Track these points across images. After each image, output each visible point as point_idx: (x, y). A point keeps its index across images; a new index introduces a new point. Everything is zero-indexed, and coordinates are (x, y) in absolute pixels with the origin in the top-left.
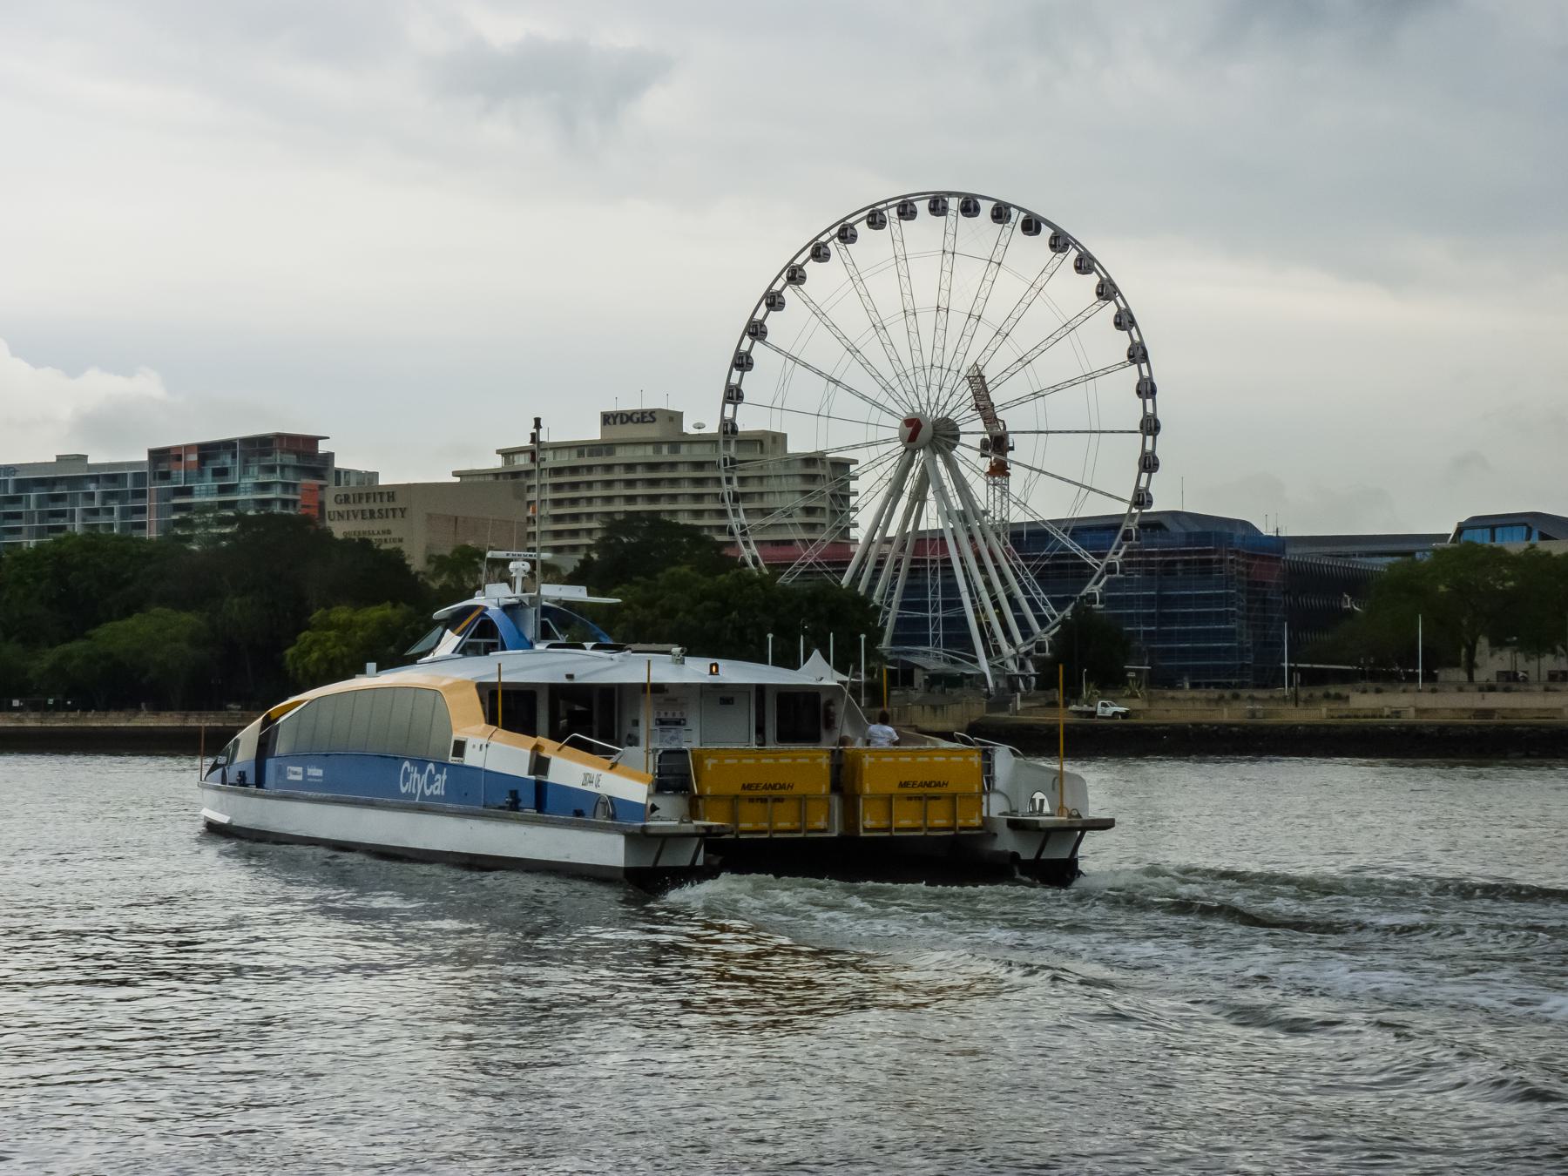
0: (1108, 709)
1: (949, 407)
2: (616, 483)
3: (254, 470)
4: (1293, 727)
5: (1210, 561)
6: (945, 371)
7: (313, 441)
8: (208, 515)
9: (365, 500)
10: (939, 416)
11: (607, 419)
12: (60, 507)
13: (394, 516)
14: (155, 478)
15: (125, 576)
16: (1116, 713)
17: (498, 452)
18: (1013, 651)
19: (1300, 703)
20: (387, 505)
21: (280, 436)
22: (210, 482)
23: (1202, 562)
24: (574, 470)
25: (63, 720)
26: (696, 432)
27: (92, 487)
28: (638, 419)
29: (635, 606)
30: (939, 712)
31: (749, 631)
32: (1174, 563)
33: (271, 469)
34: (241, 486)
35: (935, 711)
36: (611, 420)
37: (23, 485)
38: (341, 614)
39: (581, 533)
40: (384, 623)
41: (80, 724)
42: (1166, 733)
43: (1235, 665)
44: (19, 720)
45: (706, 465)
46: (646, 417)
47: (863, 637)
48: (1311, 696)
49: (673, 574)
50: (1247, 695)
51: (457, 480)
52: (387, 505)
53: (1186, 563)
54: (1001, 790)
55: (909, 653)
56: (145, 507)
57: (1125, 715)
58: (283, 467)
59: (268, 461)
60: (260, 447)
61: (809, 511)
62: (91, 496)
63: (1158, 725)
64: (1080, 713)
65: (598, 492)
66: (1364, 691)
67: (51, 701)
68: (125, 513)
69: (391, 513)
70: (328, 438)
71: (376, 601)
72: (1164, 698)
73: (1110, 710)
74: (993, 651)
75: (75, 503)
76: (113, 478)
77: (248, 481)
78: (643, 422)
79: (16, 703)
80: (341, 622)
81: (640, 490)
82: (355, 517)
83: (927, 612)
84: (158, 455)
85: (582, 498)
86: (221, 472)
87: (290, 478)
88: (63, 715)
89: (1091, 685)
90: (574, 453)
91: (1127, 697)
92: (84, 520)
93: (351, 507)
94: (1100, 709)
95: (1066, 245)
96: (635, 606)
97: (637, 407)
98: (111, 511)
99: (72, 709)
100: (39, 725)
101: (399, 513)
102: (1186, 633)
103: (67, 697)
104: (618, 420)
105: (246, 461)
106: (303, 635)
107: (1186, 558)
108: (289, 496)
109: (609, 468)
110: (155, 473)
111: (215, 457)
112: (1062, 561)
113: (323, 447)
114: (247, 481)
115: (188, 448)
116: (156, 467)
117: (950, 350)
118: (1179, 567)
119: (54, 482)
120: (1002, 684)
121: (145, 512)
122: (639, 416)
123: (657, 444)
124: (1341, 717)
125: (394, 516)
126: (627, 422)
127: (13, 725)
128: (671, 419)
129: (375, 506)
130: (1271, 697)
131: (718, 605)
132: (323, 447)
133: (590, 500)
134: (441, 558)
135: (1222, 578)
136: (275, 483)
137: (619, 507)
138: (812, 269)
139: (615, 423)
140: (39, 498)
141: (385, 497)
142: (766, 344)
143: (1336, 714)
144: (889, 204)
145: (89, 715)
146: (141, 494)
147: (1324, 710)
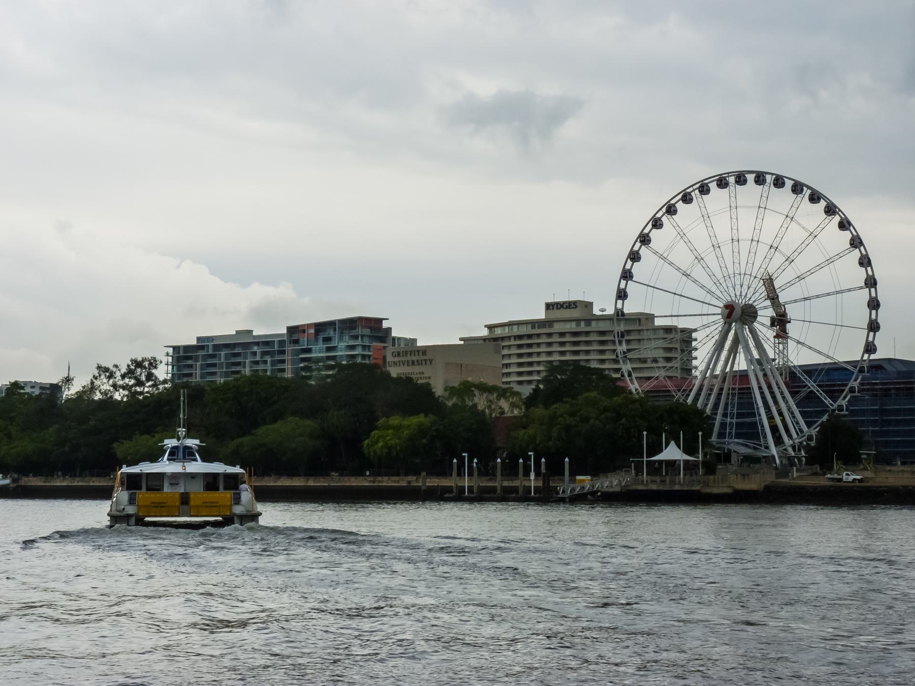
0: (850, 477)
3: (346, 338)
6: (742, 276)
7: (380, 321)
8: (320, 364)
11: (549, 306)
12: (238, 360)
13: (426, 364)
14: (290, 343)
16: (854, 479)
17: (486, 326)
18: (791, 442)
20: (422, 358)
21: (361, 319)
22: (321, 345)
23: (907, 389)
24: (530, 336)
26: (601, 313)
27: (255, 348)
28: (567, 306)
31: (632, 430)
32: (890, 389)
33: (355, 337)
34: (339, 347)
35: (744, 478)
36: (551, 307)
37: (217, 347)
38: (395, 420)
47: (700, 433)
51: (462, 342)
52: (422, 358)
53: (897, 389)
57: (860, 481)
58: (362, 336)
59: (354, 333)
60: (350, 324)
62: (255, 354)
63: (881, 487)
64: (833, 479)
65: (543, 349)
68: (274, 363)
72: (884, 470)
73: (851, 478)
76: (267, 343)
77: (342, 345)
78: (570, 308)
81: (568, 348)
82: (404, 364)
84: (292, 330)
85: (534, 353)
86: (328, 339)
89: (839, 463)
90: (530, 326)
91: (862, 470)
92: (251, 367)
94: (845, 477)
96: (565, 415)
98: (266, 362)
101: (428, 362)
104: (555, 307)
107: (898, 386)
108: (367, 353)
109: (550, 335)
110: (290, 340)
111: (324, 331)
113: (385, 325)
115: (309, 326)
116: (291, 337)
118: (893, 392)
119: (234, 346)
122: (568, 304)
123: (578, 321)
125: (426, 364)
126: (560, 308)
129: (415, 358)
132: (385, 325)
133: (539, 354)
139: (553, 309)
140: (226, 355)
141: (421, 352)
146: (283, 352)
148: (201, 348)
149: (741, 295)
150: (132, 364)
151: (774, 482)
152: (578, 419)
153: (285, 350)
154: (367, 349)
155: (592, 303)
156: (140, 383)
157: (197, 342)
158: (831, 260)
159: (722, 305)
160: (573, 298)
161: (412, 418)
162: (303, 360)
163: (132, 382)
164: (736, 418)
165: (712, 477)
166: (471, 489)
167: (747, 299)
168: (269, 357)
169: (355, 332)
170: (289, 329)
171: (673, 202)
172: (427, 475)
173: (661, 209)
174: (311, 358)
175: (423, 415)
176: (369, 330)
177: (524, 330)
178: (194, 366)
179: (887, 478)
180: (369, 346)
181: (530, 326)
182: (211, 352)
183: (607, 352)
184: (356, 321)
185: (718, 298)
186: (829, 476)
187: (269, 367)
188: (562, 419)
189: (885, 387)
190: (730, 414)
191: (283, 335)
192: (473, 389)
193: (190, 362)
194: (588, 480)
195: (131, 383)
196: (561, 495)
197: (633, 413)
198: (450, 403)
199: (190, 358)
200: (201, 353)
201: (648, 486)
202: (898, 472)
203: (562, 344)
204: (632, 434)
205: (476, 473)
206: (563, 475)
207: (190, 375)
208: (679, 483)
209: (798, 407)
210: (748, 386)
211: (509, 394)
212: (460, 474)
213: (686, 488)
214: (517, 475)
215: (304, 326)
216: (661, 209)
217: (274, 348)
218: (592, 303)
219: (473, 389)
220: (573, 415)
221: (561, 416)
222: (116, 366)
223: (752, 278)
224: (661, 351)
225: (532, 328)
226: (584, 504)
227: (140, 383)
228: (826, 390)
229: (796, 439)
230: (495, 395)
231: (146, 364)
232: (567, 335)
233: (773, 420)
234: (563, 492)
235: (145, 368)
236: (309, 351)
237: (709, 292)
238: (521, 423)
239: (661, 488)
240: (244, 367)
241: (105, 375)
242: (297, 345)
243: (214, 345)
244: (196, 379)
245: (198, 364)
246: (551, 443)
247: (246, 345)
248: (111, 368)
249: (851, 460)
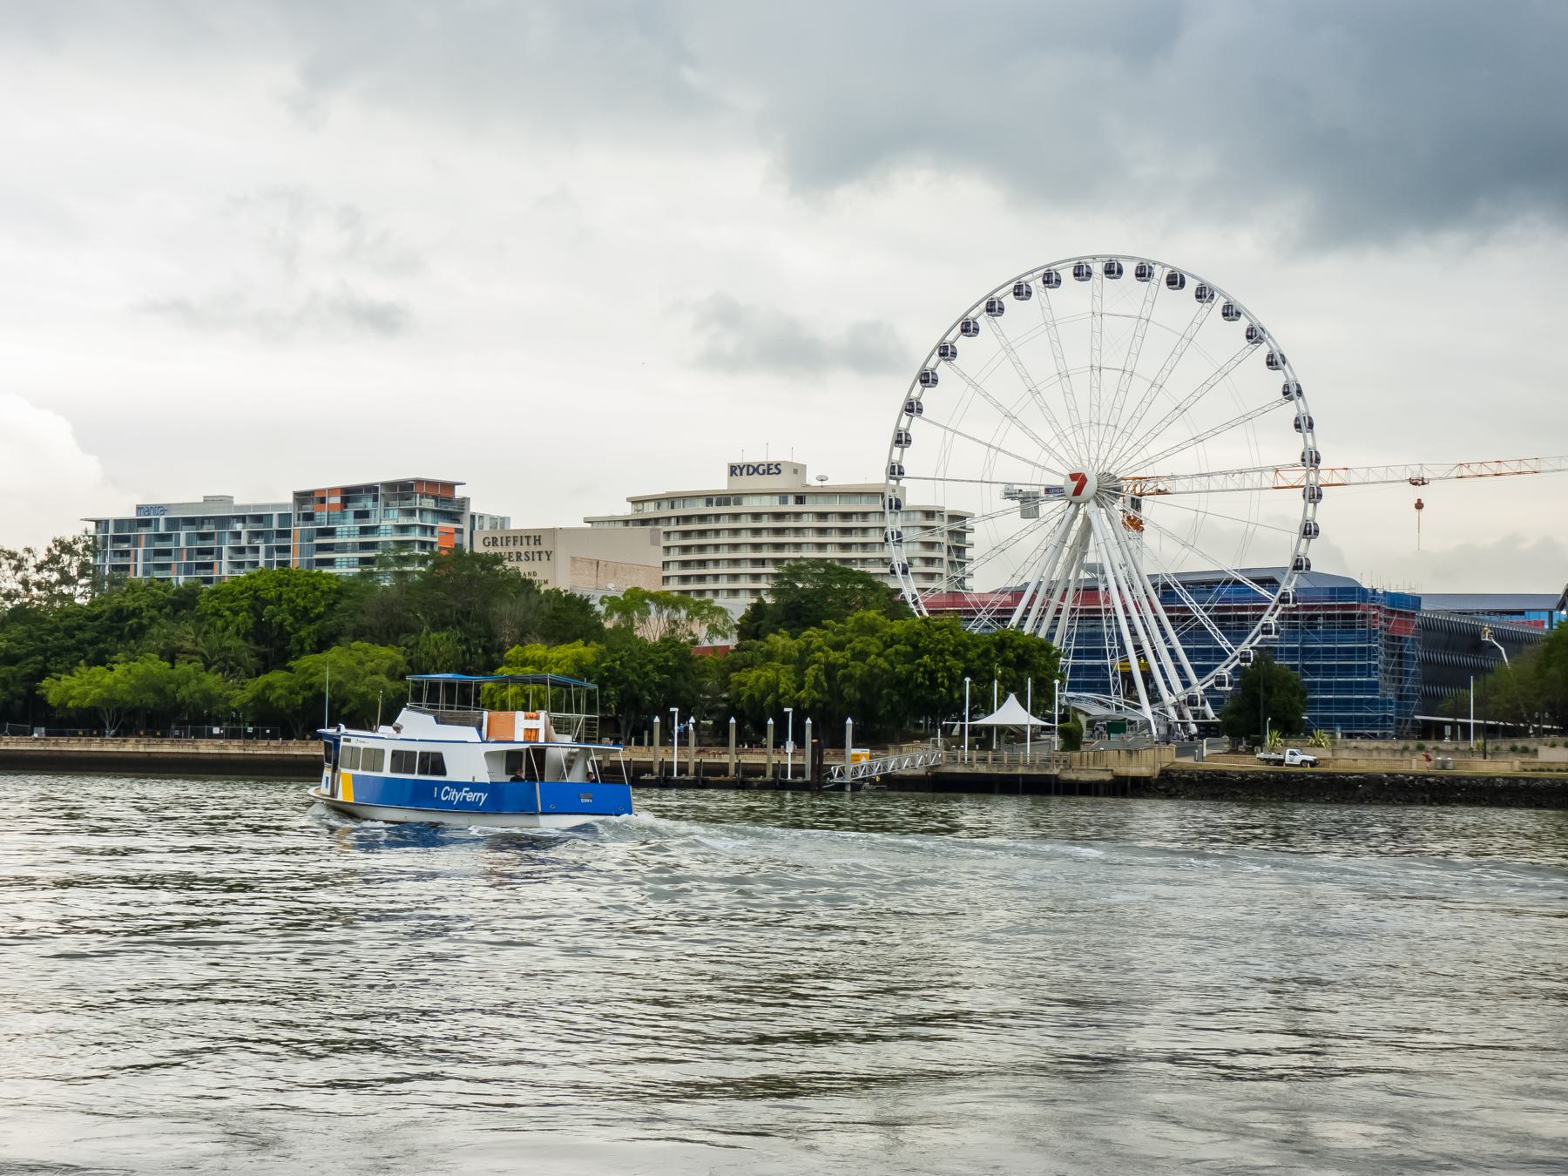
0: (1295, 756)
1: (1110, 461)
2: (743, 532)
3: (394, 513)
4: (1490, 779)
5: (1353, 616)
6: (1118, 433)
7: (450, 486)
9: (519, 543)
10: (1101, 471)
11: (734, 470)
12: (208, 545)
14: (299, 519)
15: (317, 611)
16: (1303, 761)
17: (628, 500)
18: (1174, 699)
19: (1488, 756)
20: (533, 548)
21: (419, 482)
22: (351, 524)
23: (1345, 617)
24: (702, 518)
25: (266, 748)
26: (820, 483)
27: (238, 527)
29: (826, 648)
30: (1134, 756)
31: (939, 675)
32: (1315, 617)
33: (411, 513)
35: (1131, 757)
36: (738, 471)
37: (173, 523)
38: (537, 650)
39: (708, 578)
40: (578, 661)
41: (281, 752)
42: (1359, 781)
43: (1377, 717)
44: (221, 746)
45: (829, 516)
46: (772, 469)
48: (1497, 749)
49: (862, 618)
50: (1431, 747)
51: (589, 525)
52: (533, 548)
53: (1329, 617)
55: (1079, 699)
57: (1313, 764)
58: (422, 511)
59: (407, 505)
60: (402, 490)
61: (929, 561)
62: (237, 535)
63: (1352, 774)
64: (1268, 761)
65: (724, 539)
66: (1553, 745)
67: (250, 730)
70: (464, 484)
71: (564, 640)
72: (1347, 748)
73: (1298, 759)
74: (1154, 698)
75: (136, 544)
76: (258, 519)
78: (769, 473)
79: (216, 730)
80: (536, 658)
81: (765, 538)
83: (1106, 659)
84: (302, 498)
85: (710, 545)
87: (429, 521)
88: (265, 743)
89: (1275, 733)
90: (776, 499)
91: (1311, 746)
92: (230, 558)
94: (1288, 758)
95: (1238, 314)
96: (826, 648)
97: (762, 459)
98: (256, 550)
99: (273, 737)
100: (242, 752)
101: (544, 556)
102: (1329, 684)
103: (268, 725)
104: (745, 471)
105: (387, 505)
106: (500, 670)
107: (1329, 612)
108: (428, 538)
109: (736, 516)
110: (299, 515)
111: (357, 500)
112: (1244, 613)
113: (459, 493)
114: (387, 523)
115: (332, 491)
117: (1127, 413)
118: (1321, 620)
120: (1163, 730)
121: (289, 551)
122: (766, 468)
123: (783, 497)
124: (1533, 770)
127: (217, 751)
128: (795, 471)
129: (523, 549)
130: (1457, 749)
131: (909, 649)
132: (459, 493)
133: (717, 547)
134: (613, 599)
135: (1365, 632)
136: (415, 525)
137: (831, 554)
138: (963, 344)
139: (741, 474)
142: (924, 419)
143: (1529, 767)
144: (1035, 274)
145: (291, 743)
146: (286, 534)
147: (1517, 763)
148: (146, 523)
149: (1097, 460)
150: (56, 546)
151: (1173, 763)
152: (848, 654)
154: (429, 532)
155: (804, 467)
156: (66, 579)
159: (1067, 473)
160: (773, 459)
161: (562, 647)
162: (321, 548)
163: (55, 576)
164: (1073, 659)
165: (1077, 755)
166: (683, 769)
167: (1101, 462)
168: (262, 541)
169: (411, 505)
171: (997, 295)
172: (48, 734)
173: (977, 305)
174: (333, 544)
175: (581, 642)
176: (433, 501)
177: (700, 508)
178: (132, 554)
179: (1355, 760)
180: (432, 529)
181: (776, 499)
182: (162, 530)
183: (764, 547)
185: (1060, 460)
186: (1262, 755)
187: (262, 559)
188: (821, 654)
189: (1309, 612)
190: (1110, 650)
191: (284, 506)
192: (647, 601)
193: (125, 547)
194: (865, 755)
195: (53, 580)
196: (836, 780)
197: (940, 646)
198: (608, 625)
199: (126, 539)
200: (144, 532)
201: (972, 766)
202: (1370, 751)
203: (756, 531)
204: (939, 680)
205: (692, 739)
207: (210, 566)
208: (1025, 765)
209: (1182, 642)
211: (706, 612)
212: (779, 743)
213: (1035, 772)
214: (726, 744)
215: (323, 491)
216: (977, 305)
218: (804, 467)
219: (647, 601)
220: (838, 647)
221: (819, 649)
222: (29, 550)
223: (1118, 433)
224: (918, 547)
225: (797, 503)
226: (254, 780)
227: (66, 579)
228: (1215, 616)
229: (1181, 694)
230: (683, 613)
231: (79, 547)
232: (765, 517)
233: (1127, 664)
234: (840, 775)
235: (76, 554)
236: (330, 532)
237: (1046, 448)
238: (733, 663)
239: (995, 771)
240: (220, 557)
241: (10, 564)
242: (310, 522)
243: (167, 520)
245: (140, 550)
246: (803, 694)
247: (223, 521)
248: (21, 553)
249: (1291, 729)
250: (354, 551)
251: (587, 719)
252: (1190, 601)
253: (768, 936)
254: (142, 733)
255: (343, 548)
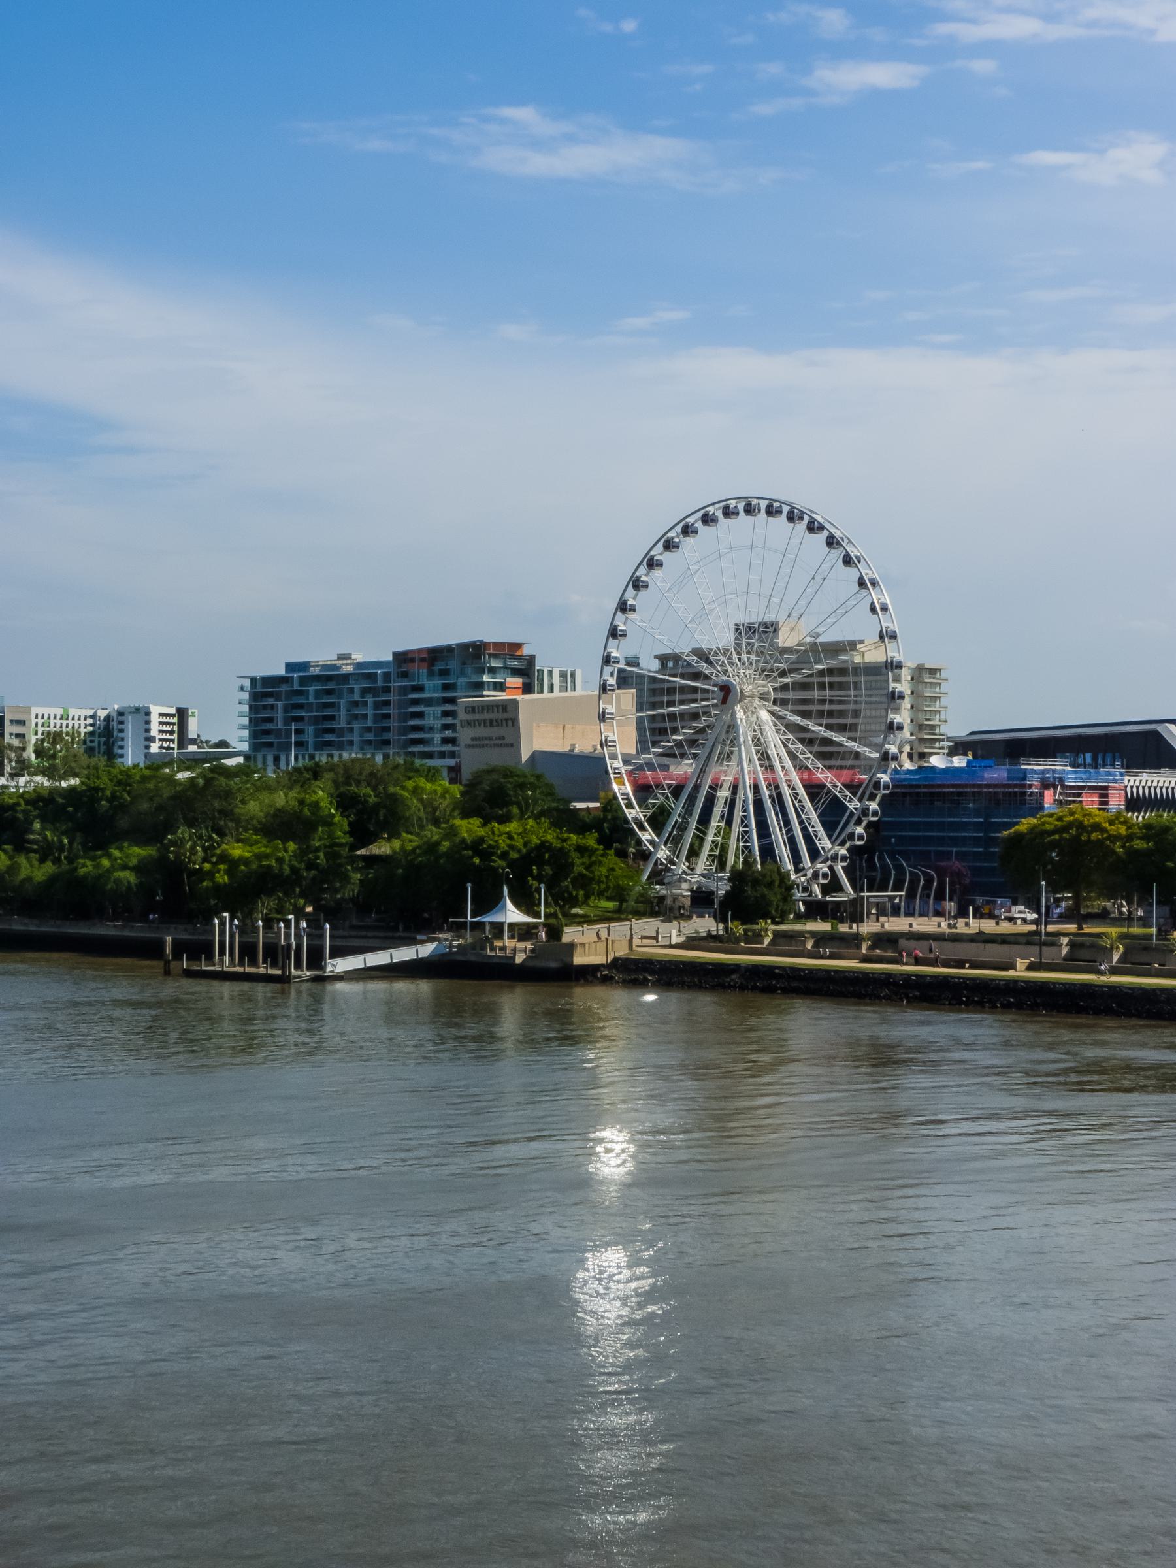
7: (519, 646)
14: (398, 677)
17: (656, 657)
52: (501, 716)
54: (600, 991)
56: (390, 701)
68: (377, 706)
69: (504, 722)
82: (480, 725)
84: (403, 658)
92: (348, 710)
93: (477, 717)
101: (510, 723)
116: (399, 667)
132: (526, 651)
140: (317, 691)
146: (387, 690)
153: (390, 687)
157: (286, 671)
158: (840, 611)
170: (395, 655)
182: (296, 687)
184: (413, 660)
187: (370, 712)
193: (271, 701)
199: (270, 695)
200: (284, 688)
206: (968, 915)
207: (332, 718)
210: (506, 928)
217: (376, 682)
236: (420, 689)
244: (574, 689)
245: (280, 704)
250: (439, 704)
251: (974, 917)
252: (834, 836)
253: (982, 1517)
254: (338, 885)
255: (429, 702)
